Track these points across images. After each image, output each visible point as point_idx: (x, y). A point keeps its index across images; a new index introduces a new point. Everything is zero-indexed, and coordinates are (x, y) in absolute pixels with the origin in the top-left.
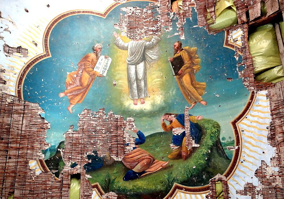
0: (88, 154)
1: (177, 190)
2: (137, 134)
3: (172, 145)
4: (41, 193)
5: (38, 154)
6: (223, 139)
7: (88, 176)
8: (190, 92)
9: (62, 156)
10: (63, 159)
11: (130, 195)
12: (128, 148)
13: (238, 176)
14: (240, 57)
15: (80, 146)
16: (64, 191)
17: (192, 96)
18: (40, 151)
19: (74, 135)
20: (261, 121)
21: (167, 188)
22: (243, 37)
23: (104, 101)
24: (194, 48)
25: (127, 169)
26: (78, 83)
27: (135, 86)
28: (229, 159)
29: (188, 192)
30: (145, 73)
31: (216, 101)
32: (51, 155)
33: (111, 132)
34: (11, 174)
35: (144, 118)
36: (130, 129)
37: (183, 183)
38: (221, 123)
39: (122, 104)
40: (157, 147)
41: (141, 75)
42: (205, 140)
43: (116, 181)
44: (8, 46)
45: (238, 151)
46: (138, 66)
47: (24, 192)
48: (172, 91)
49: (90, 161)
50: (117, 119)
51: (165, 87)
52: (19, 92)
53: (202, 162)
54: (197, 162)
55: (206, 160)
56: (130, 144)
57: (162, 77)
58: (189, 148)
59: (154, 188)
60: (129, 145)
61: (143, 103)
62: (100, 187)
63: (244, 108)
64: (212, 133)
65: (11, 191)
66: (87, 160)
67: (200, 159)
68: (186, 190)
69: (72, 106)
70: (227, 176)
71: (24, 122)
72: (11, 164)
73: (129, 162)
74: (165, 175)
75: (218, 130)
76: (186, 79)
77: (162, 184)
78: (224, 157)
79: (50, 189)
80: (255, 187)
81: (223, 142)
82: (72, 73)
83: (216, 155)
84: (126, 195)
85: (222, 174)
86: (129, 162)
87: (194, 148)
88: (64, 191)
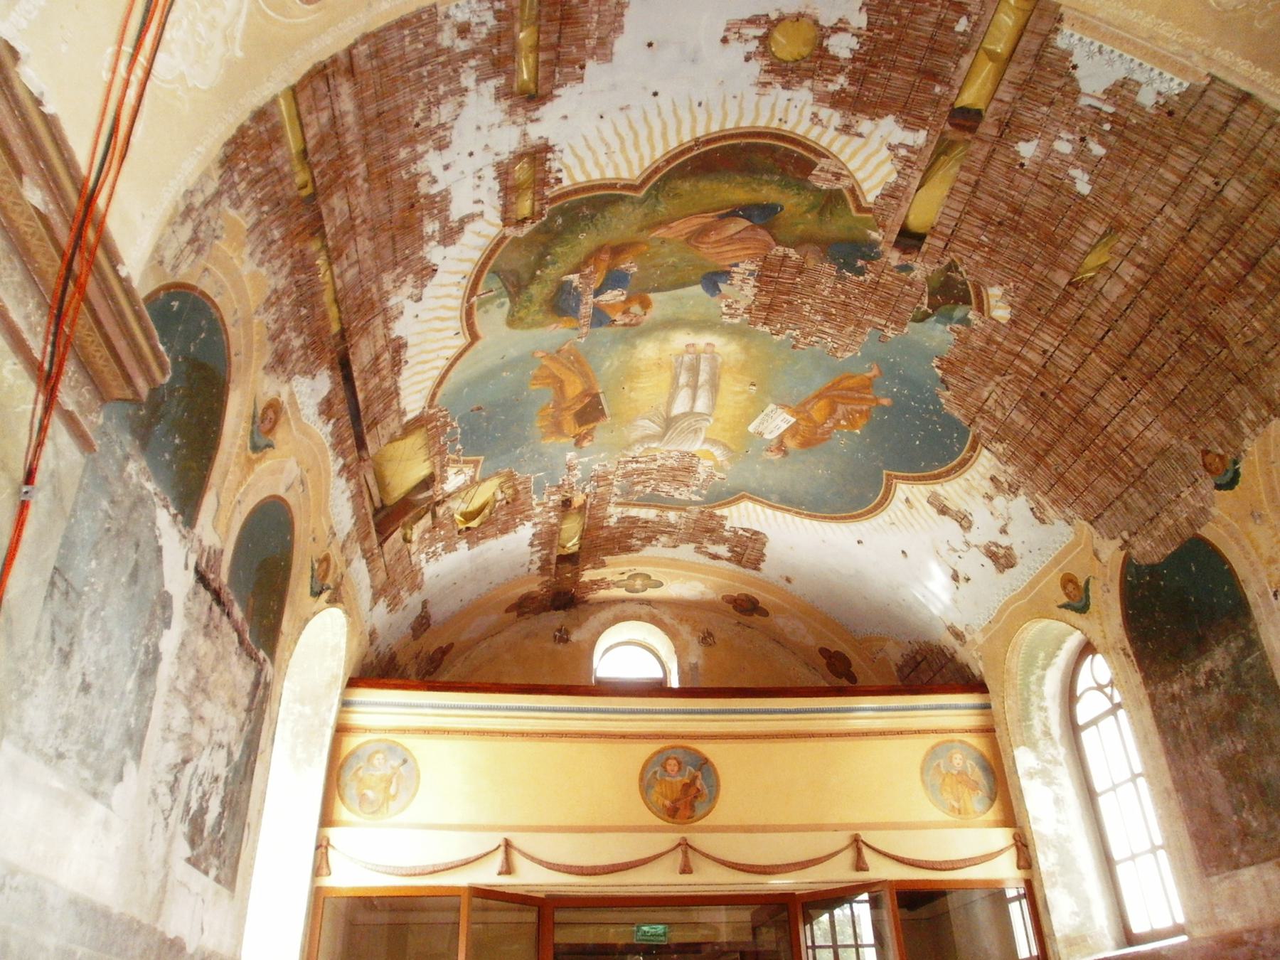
0: (861, 278)
1: (638, 183)
7: (875, 235)
8: (569, 369)
10: (927, 289)
12: (752, 267)
15: (876, 298)
16: (947, 226)
19: (883, 322)
20: (416, 378)
21: (665, 184)
25: (768, 228)
26: (841, 409)
27: (703, 377)
28: (494, 272)
29: (608, 182)
31: (510, 365)
32: (954, 310)
33: (790, 303)
34: (1057, 321)
35: (693, 318)
36: (737, 302)
37: (622, 198)
39: (746, 349)
40: (674, 265)
43: (804, 209)
44: (961, 525)
46: (687, 409)
47: (1045, 272)
49: (860, 263)
50: (765, 324)
51: (630, 374)
52: (973, 448)
53: (559, 250)
59: (701, 185)
60: (747, 272)
62: (852, 206)
63: (451, 374)
65: (1072, 290)
69: (868, 375)
70: (504, 238)
71: (986, 394)
72: (1048, 339)
73: (758, 240)
75: (513, 315)
76: (574, 387)
77: (678, 191)
79: (984, 246)
81: (502, 300)
84: (784, 172)
86: (758, 240)
88: (947, 226)
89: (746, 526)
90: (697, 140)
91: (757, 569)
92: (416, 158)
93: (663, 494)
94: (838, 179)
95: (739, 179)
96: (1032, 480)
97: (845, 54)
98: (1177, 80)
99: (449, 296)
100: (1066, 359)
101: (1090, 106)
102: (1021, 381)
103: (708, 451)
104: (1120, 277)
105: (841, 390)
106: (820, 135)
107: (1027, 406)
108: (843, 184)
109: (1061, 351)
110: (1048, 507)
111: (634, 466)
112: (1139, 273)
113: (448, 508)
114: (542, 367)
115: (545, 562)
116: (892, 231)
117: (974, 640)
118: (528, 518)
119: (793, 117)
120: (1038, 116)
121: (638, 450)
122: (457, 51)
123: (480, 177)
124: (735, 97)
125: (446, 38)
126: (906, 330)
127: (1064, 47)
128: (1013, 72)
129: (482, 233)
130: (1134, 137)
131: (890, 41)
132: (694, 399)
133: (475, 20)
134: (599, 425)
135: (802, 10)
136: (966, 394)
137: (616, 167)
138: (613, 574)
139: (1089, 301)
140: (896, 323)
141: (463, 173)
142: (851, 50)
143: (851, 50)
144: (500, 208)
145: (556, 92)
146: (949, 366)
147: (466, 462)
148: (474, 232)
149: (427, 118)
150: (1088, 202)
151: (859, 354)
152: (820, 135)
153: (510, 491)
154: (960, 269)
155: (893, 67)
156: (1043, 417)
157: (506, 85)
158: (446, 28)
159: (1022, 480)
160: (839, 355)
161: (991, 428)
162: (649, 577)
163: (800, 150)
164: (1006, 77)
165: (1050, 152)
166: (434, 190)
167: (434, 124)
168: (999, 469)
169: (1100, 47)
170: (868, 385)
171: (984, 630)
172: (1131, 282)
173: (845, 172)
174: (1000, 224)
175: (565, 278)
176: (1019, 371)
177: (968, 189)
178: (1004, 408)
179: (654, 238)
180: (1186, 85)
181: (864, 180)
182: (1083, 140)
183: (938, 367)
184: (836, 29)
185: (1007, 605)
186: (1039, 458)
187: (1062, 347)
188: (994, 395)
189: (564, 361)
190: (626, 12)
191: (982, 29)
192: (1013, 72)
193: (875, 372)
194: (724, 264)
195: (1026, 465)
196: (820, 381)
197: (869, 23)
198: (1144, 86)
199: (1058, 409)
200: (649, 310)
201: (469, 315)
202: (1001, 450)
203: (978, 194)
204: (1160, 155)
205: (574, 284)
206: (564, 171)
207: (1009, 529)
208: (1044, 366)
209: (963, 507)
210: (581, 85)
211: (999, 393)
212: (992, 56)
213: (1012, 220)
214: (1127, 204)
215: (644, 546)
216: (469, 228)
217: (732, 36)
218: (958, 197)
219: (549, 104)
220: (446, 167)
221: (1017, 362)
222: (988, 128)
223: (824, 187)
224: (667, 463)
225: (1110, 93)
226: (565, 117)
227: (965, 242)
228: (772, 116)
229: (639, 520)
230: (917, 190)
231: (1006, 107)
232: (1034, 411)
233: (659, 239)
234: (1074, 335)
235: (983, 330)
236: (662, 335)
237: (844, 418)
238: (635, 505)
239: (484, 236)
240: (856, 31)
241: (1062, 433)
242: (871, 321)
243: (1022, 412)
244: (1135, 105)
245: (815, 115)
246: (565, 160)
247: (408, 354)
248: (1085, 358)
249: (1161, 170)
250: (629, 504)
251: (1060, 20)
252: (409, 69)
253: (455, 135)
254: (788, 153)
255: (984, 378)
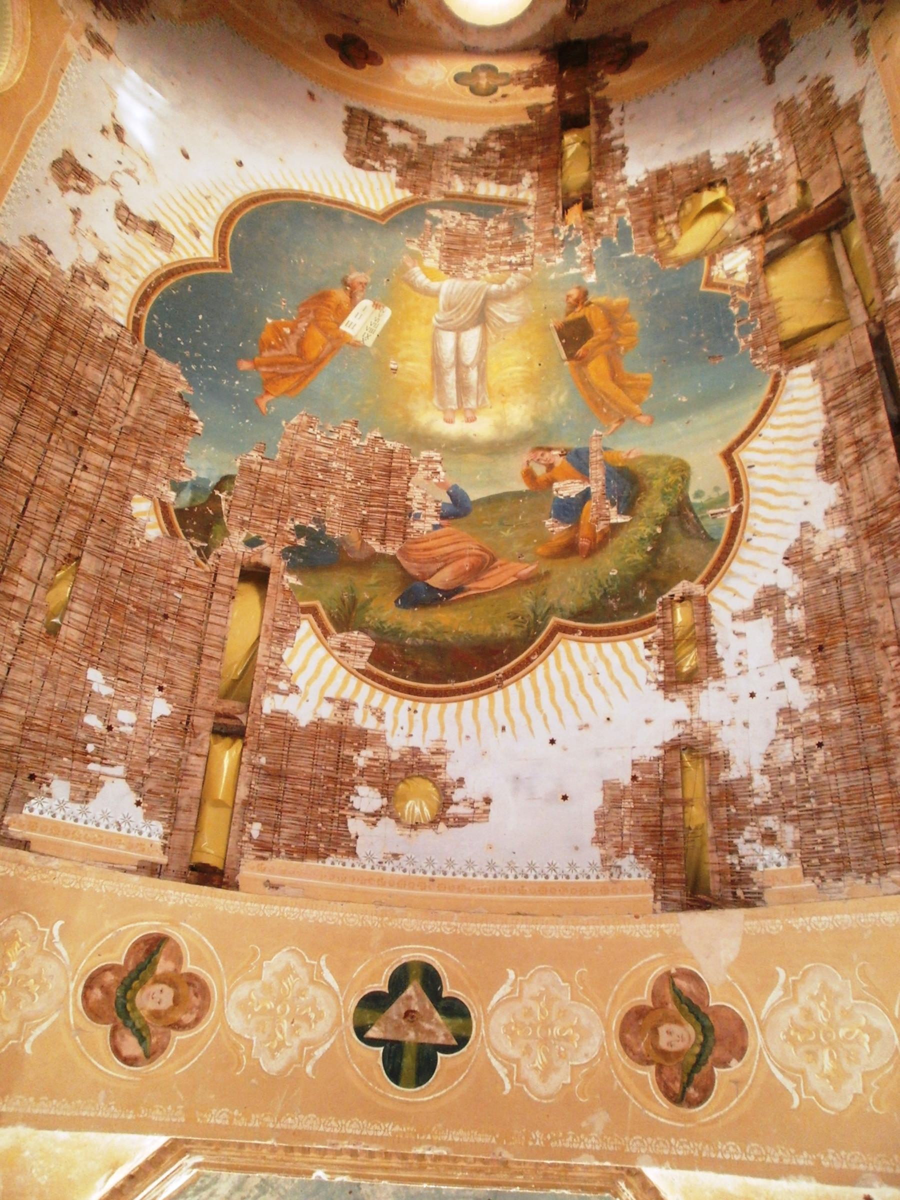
0: (297, 523)
1: (559, 635)
2: (448, 493)
3: (548, 523)
4: (152, 588)
5: (159, 486)
6: (698, 494)
7: (292, 579)
9: (225, 512)
10: (225, 519)
11: (412, 647)
12: (417, 525)
13: (738, 576)
14: (743, 306)
15: (277, 499)
16: (219, 603)
17: (613, 406)
18: (165, 482)
19: (264, 469)
20: (797, 433)
21: (528, 631)
22: (750, 266)
23: (358, 403)
24: (620, 300)
25: (407, 578)
26: (292, 348)
27: (451, 378)
28: (712, 539)
29: (592, 638)
30: (483, 351)
31: (677, 412)
32: (193, 500)
33: (369, 481)
34: (81, 511)
35: (471, 457)
36: (428, 479)
37: (575, 617)
38: (691, 459)
39: (408, 417)
41: (470, 354)
42: (647, 504)
43: (372, 605)
44: (127, 209)
45: (738, 514)
48: (559, 394)
49: (302, 542)
50: (392, 451)
52: (137, 322)
53: (638, 557)
54: (623, 559)
55: (648, 553)
56: (425, 516)
57: (529, 363)
58: (601, 526)
60: (422, 518)
61: (472, 420)
62: (323, 613)
64: (668, 486)
65: (75, 552)
66: (292, 538)
67: (631, 551)
68: (587, 632)
69: (269, 398)
70: (705, 583)
71: (137, 397)
72: (84, 485)
74: (526, 599)
75: (683, 478)
76: (597, 368)
77: (514, 622)
78: (699, 538)
80: (783, 593)
81: (698, 501)
82: (281, 323)
83: (678, 536)
84: (402, 647)
85: (692, 580)
86: (416, 561)
87: (615, 528)
88: (219, 603)
89: (372, 175)
90: (501, 687)
91: (350, 109)
92: (817, 705)
93: (473, 217)
94: (343, 644)
95: (449, 638)
96: (59, 293)
97: (363, 790)
98: (36, 813)
99: (766, 521)
100: (60, 466)
101: (113, 766)
102: (101, 424)
103: (432, 280)
104: (29, 580)
105: (294, 374)
106: (371, 697)
107: (87, 392)
108: (337, 639)
109: (68, 474)
110: (32, 260)
111: (513, 259)
112: (11, 590)
113: (745, 223)
114: (638, 401)
115: (604, 123)
116: (275, 586)
117: (77, 39)
118: (633, 192)
119: (403, 715)
120: (158, 745)
121: (513, 281)
122: (776, 817)
123: (740, 664)
124: (468, 737)
125: (790, 833)
126: (238, 463)
127: (154, 822)
128: (194, 787)
129: (731, 593)
130: (61, 742)
131: (321, 806)
132: (458, 350)
133: (757, 846)
134: (562, 319)
135: (413, 833)
136: (158, 393)
137: (585, 656)
138: (516, 97)
139: (54, 543)
140: (251, 471)
141: (761, 675)
142: (357, 794)
143: (357, 794)
144: (712, 621)
145: (660, 753)
146: (182, 425)
147: (724, 287)
148: (742, 597)
149: (809, 750)
150: (85, 660)
151: (284, 423)
152: (371, 697)
153: (661, 234)
154: (195, 553)
155: (312, 778)
156: (67, 383)
157: (718, 769)
158: (790, 844)
159: (71, 291)
160: (305, 419)
161: (122, 354)
162: (473, 90)
163: (390, 677)
164: (201, 780)
165: (137, 708)
166: (794, 661)
167: (799, 740)
168: (101, 300)
169: (119, 830)
170: (268, 384)
171: (66, 56)
172: (16, 577)
173: (337, 653)
174: (166, 616)
175: (627, 519)
176: (107, 436)
177: (207, 651)
178: (114, 385)
179: (531, 563)
180: (26, 811)
181: (316, 646)
182: (110, 728)
183: (196, 421)
184: (377, 815)
185: (48, 103)
186: (57, 326)
187: (68, 479)
188: (127, 397)
189: (613, 406)
190: (594, 834)
191: (235, 828)
192: (194, 787)
193: (263, 403)
194: (449, 529)
195: (72, 313)
196: (321, 382)
197: (346, 823)
198: (67, 800)
199: (52, 398)
200: (525, 467)
201: (738, 492)
202: (105, 327)
203: (195, 647)
204: (30, 730)
205: (615, 509)
206: (643, 658)
207: (70, 217)
208: (81, 449)
209: (130, 238)
210: (636, 757)
211: (123, 402)
212: (218, 804)
213: (155, 623)
214: (46, 666)
215: (485, 139)
216: (748, 604)
217: (481, 805)
218: (215, 640)
219: (667, 739)
220: (781, 686)
221: (111, 447)
222: (203, 722)
223: (356, 632)
224: (475, 261)
225: (96, 784)
226: (648, 721)
227: (197, 587)
228: (425, 717)
229: (496, 179)
230: (258, 638)
231: (192, 749)
232: (78, 388)
233: (525, 562)
234: (59, 497)
235: (156, 480)
236: (506, 435)
237: (286, 336)
238: (503, 201)
239: (730, 589)
240: (357, 814)
241: (40, 367)
242: (278, 468)
243: (93, 384)
244: (70, 778)
245: (380, 719)
246: (643, 671)
247: (814, 456)
248: (39, 473)
249: (23, 713)
250: (511, 202)
251: (164, 847)
252: (831, 810)
253: (773, 722)
254: (401, 673)
255: (144, 418)
